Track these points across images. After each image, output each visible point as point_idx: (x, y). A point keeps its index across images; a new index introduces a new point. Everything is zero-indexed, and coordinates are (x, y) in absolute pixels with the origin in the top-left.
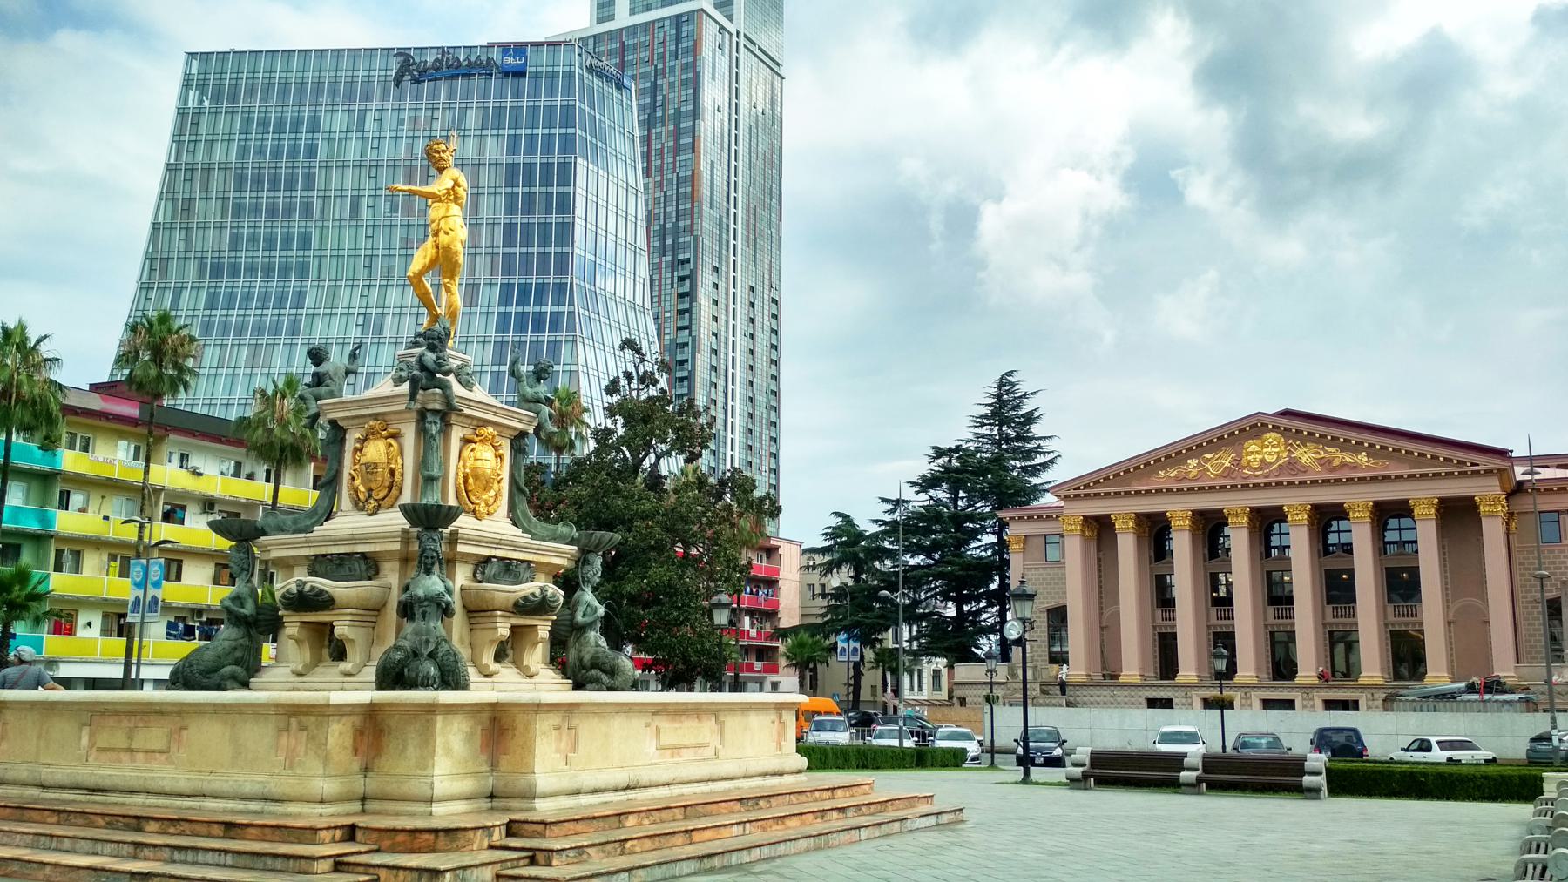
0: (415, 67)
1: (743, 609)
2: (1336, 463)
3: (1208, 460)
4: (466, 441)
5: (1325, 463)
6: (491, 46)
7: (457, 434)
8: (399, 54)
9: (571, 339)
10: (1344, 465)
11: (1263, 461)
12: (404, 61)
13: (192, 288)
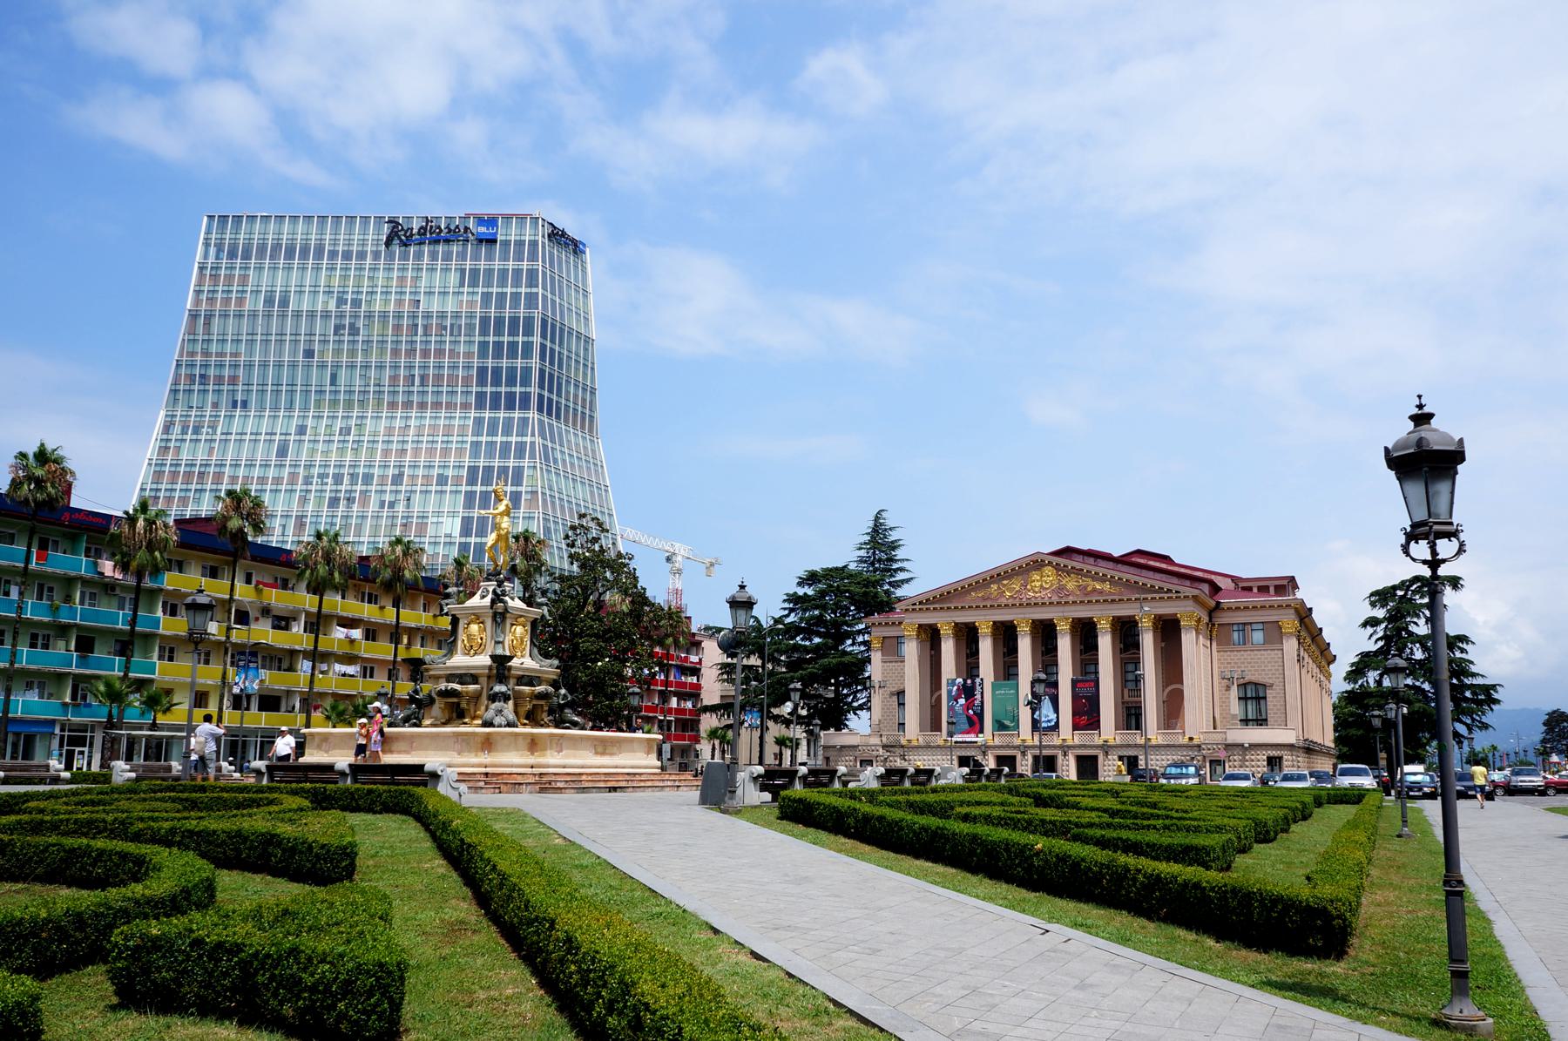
0: (403, 233)
1: (670, 691)
2: (1089, 589)
3: (1004, 585)
4: (513, 625)
5: (1082, 588)
6: (467, 217)
7: (508, 622)
8: (389, 222)
9: (532, 464)
10: (1094, 590)
11: (1041, 586)
12: (394, 227)
13: (260, 465)
